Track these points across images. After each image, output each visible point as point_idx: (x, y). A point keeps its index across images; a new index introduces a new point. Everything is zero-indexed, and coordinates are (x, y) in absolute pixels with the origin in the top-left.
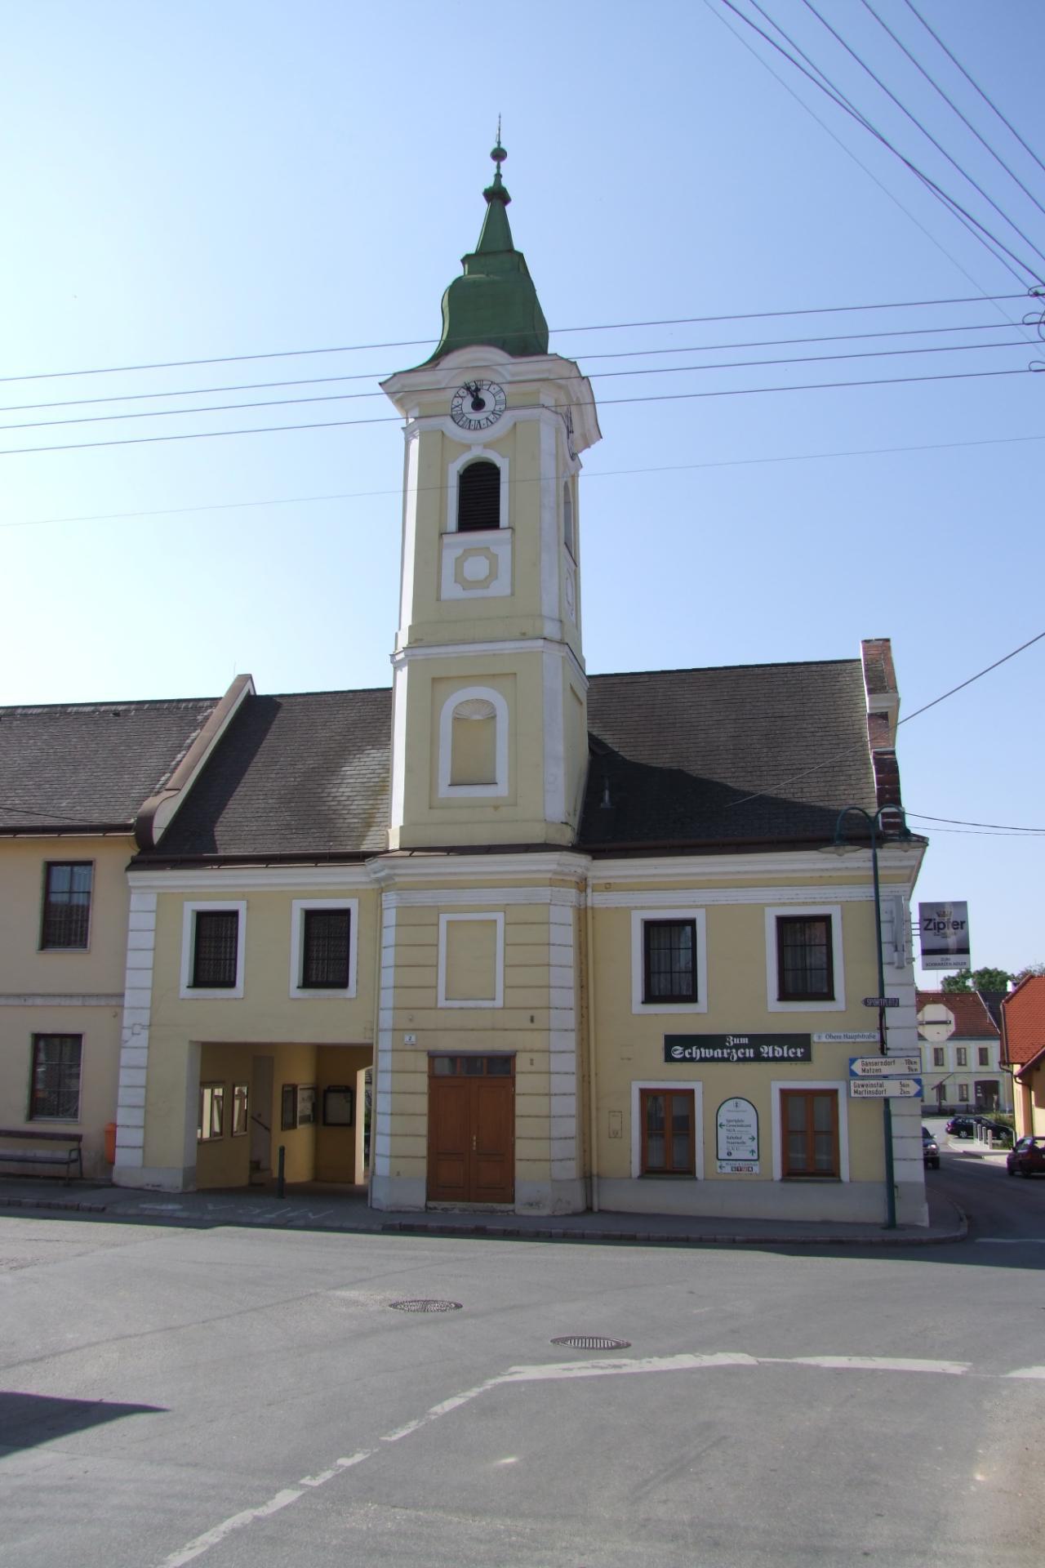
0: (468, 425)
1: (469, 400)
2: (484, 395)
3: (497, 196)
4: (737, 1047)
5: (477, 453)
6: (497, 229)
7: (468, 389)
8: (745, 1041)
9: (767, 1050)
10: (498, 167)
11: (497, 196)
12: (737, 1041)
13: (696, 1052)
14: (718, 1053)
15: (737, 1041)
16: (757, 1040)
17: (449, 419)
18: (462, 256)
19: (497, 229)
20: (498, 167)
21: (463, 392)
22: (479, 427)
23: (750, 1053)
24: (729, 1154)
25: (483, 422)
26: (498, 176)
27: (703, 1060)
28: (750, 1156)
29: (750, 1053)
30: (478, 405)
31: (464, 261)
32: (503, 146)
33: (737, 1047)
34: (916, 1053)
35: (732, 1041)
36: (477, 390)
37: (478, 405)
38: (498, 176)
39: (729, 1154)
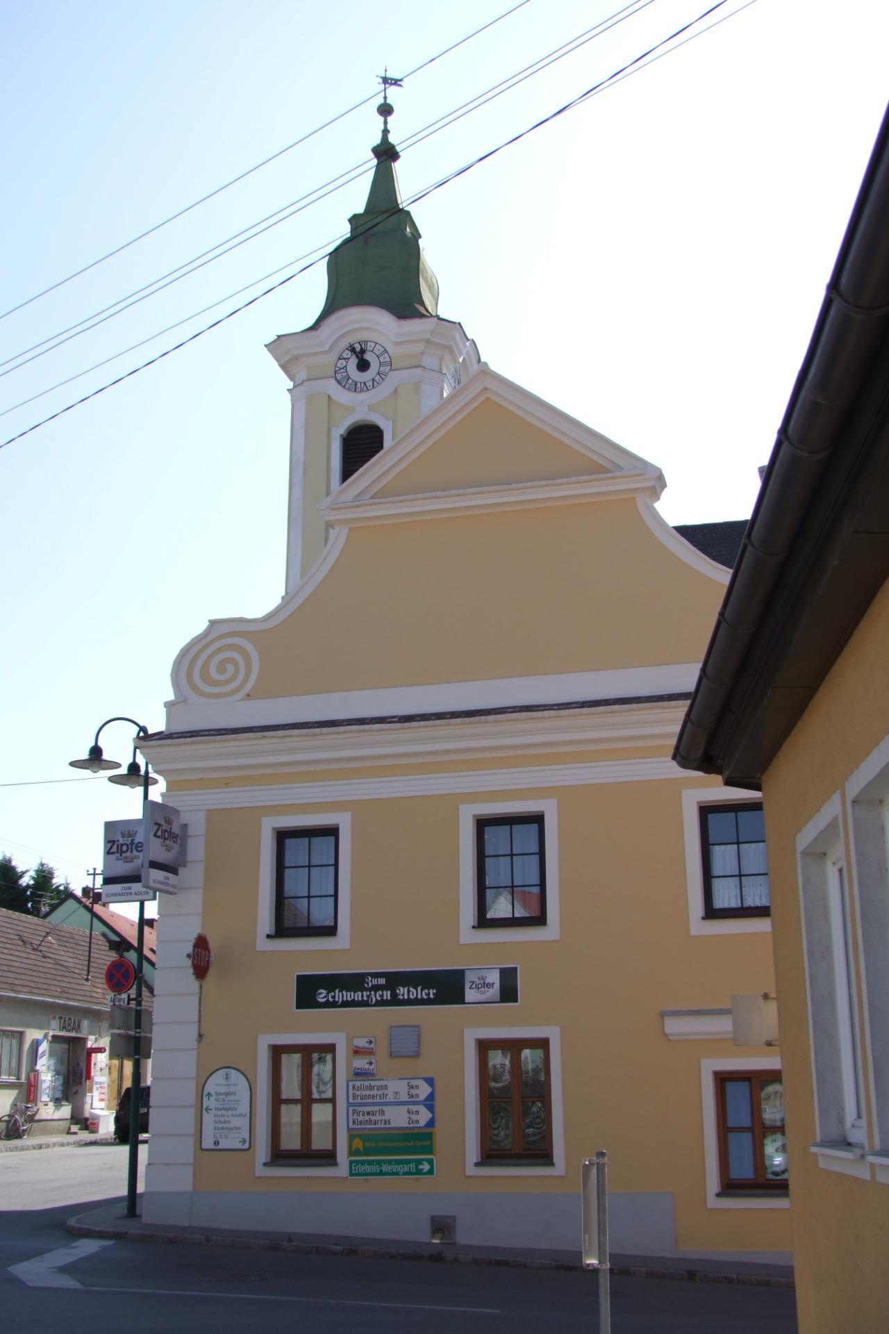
0: (355, 388)
1: (354, 361)
2: (367, 357)
3: (386, 153)
4: (376, 988)
5: (362, 415)
6: (383, 185)
7: (353, 350)
8: (382, 981)
9: (402, 992)
10: (386, 123)
11: (386, 153)
12: (375, 982)
13: (339, 996)
14: (358, 996)
15: (375, 982)
16: (395, 980)
17: (333, 382)
18: (350, 215)
19: (383, 185)
20: (386, 123)
21: (347, 354)
22: (365, 388)
23: (387, 995)
24: (217, 1143)
25: (369, 384)
26: (386, 132)
27: (346, 1004)
28: (239, 1146)
29: (387, 995)
30: (363, 366)
31: (350, 220)
32: (389, 101)
33: (376, 988)
34: (291, 1063)
35: (372, 982)
36: (363, 351)
37: (363, 366)
38: (386, 132)
39: (217, 1143)
